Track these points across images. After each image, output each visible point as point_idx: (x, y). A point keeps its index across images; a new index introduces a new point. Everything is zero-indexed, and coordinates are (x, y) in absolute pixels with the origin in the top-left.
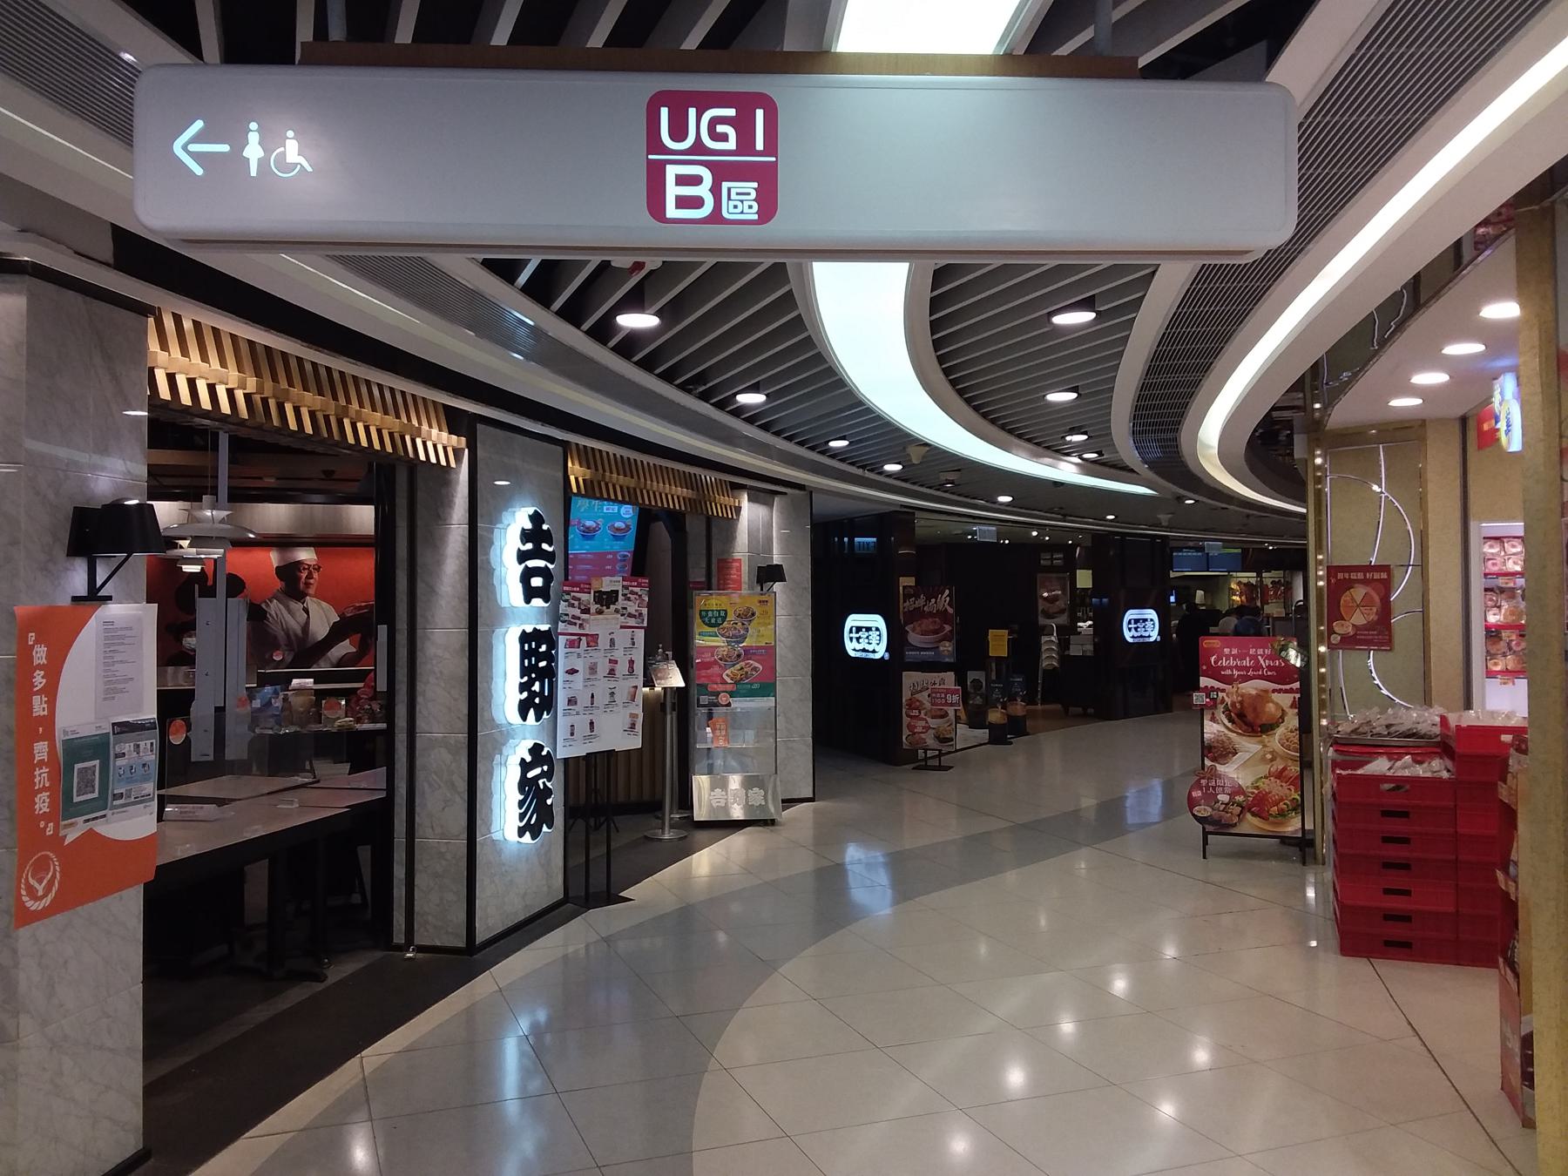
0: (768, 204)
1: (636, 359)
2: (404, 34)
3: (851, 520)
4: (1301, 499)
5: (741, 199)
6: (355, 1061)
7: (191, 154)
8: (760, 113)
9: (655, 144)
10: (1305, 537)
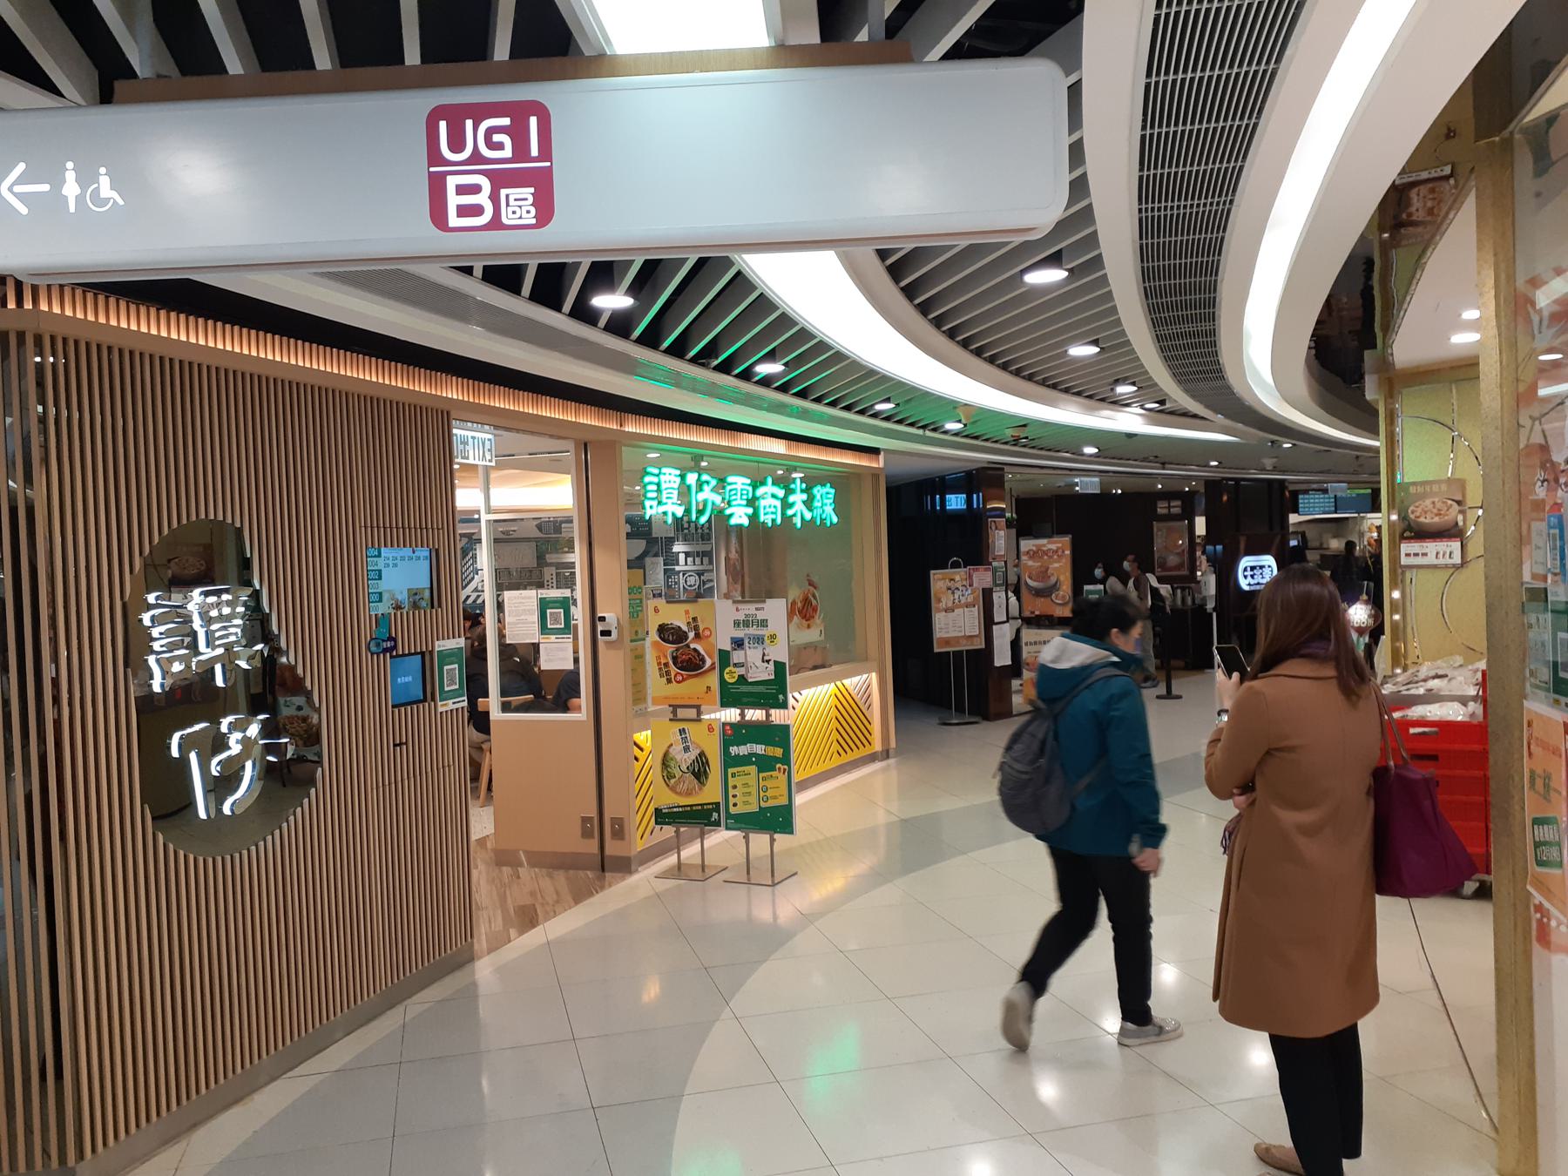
1: (667, 343)
2: (502, 49)
3: (942, 478)
4: (1373, 431)
5: (519, 204)
7: (15, 195)
8: (533, 121)
9: (435, 157)
10: (1378, 473)
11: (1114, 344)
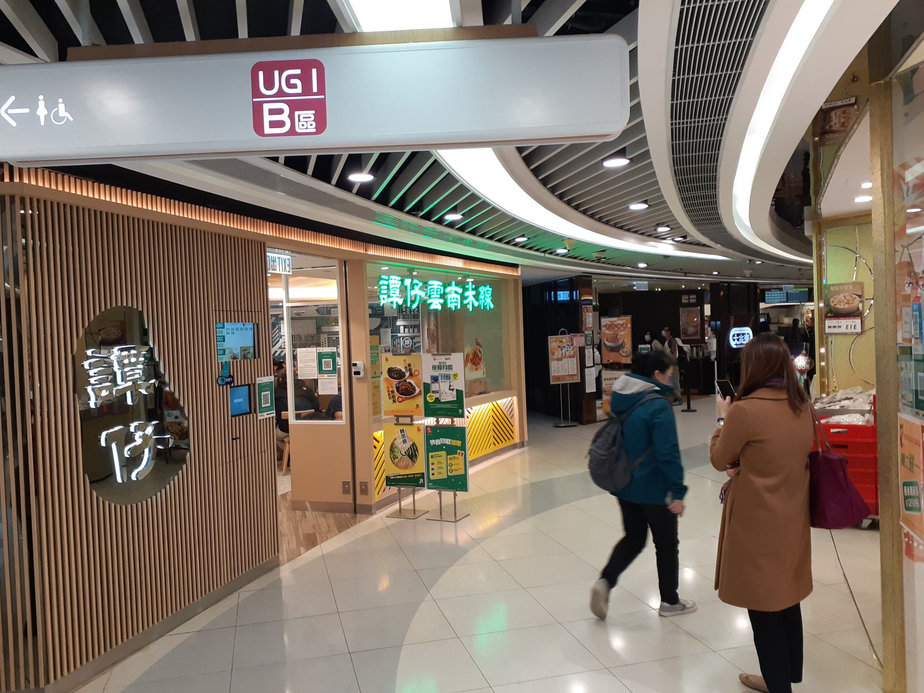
3: (555, 282)
5: (306, 120)
6: (236, 594)
7: (9, 115)
8: (314, 71)
9: (256, 92)
10: (812, 279)
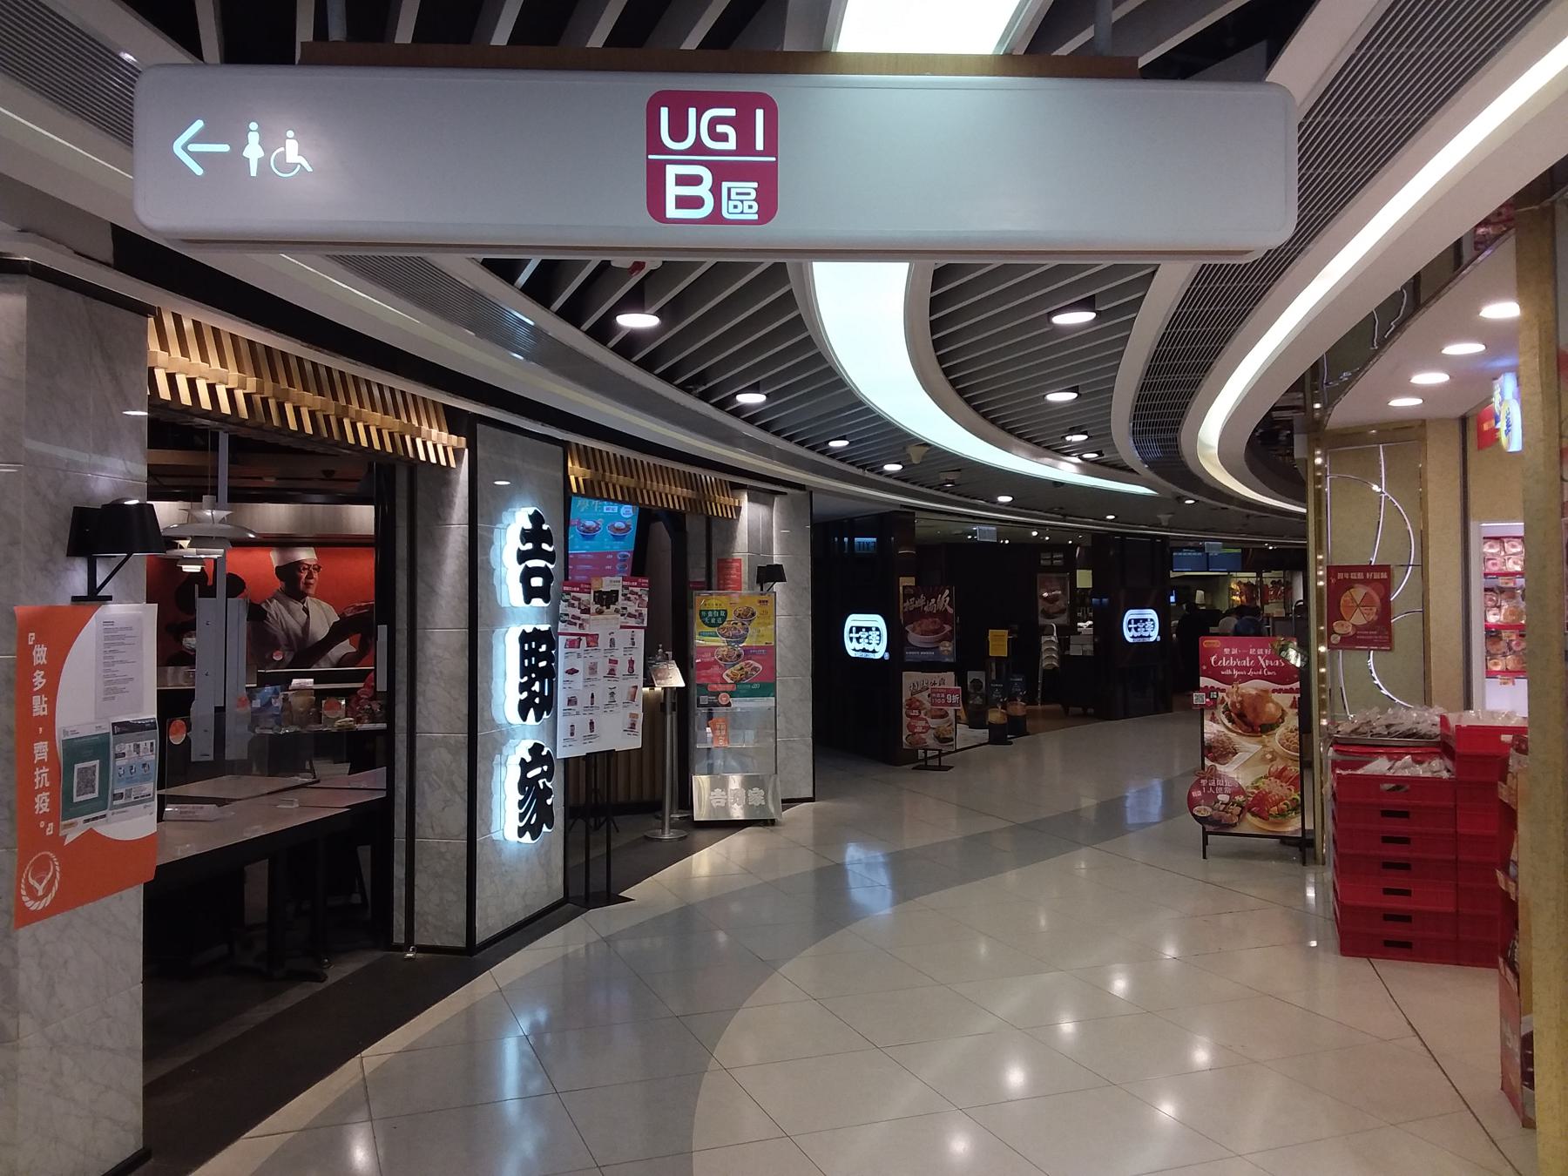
0: (768, 204)
3: (851, 520)
5: (741, 199)
6: (355, 1061)
7: (191, 154)
8: (760, 113)
9: (655, 144)
10: (1305, 537)
11: (1095, 395)
